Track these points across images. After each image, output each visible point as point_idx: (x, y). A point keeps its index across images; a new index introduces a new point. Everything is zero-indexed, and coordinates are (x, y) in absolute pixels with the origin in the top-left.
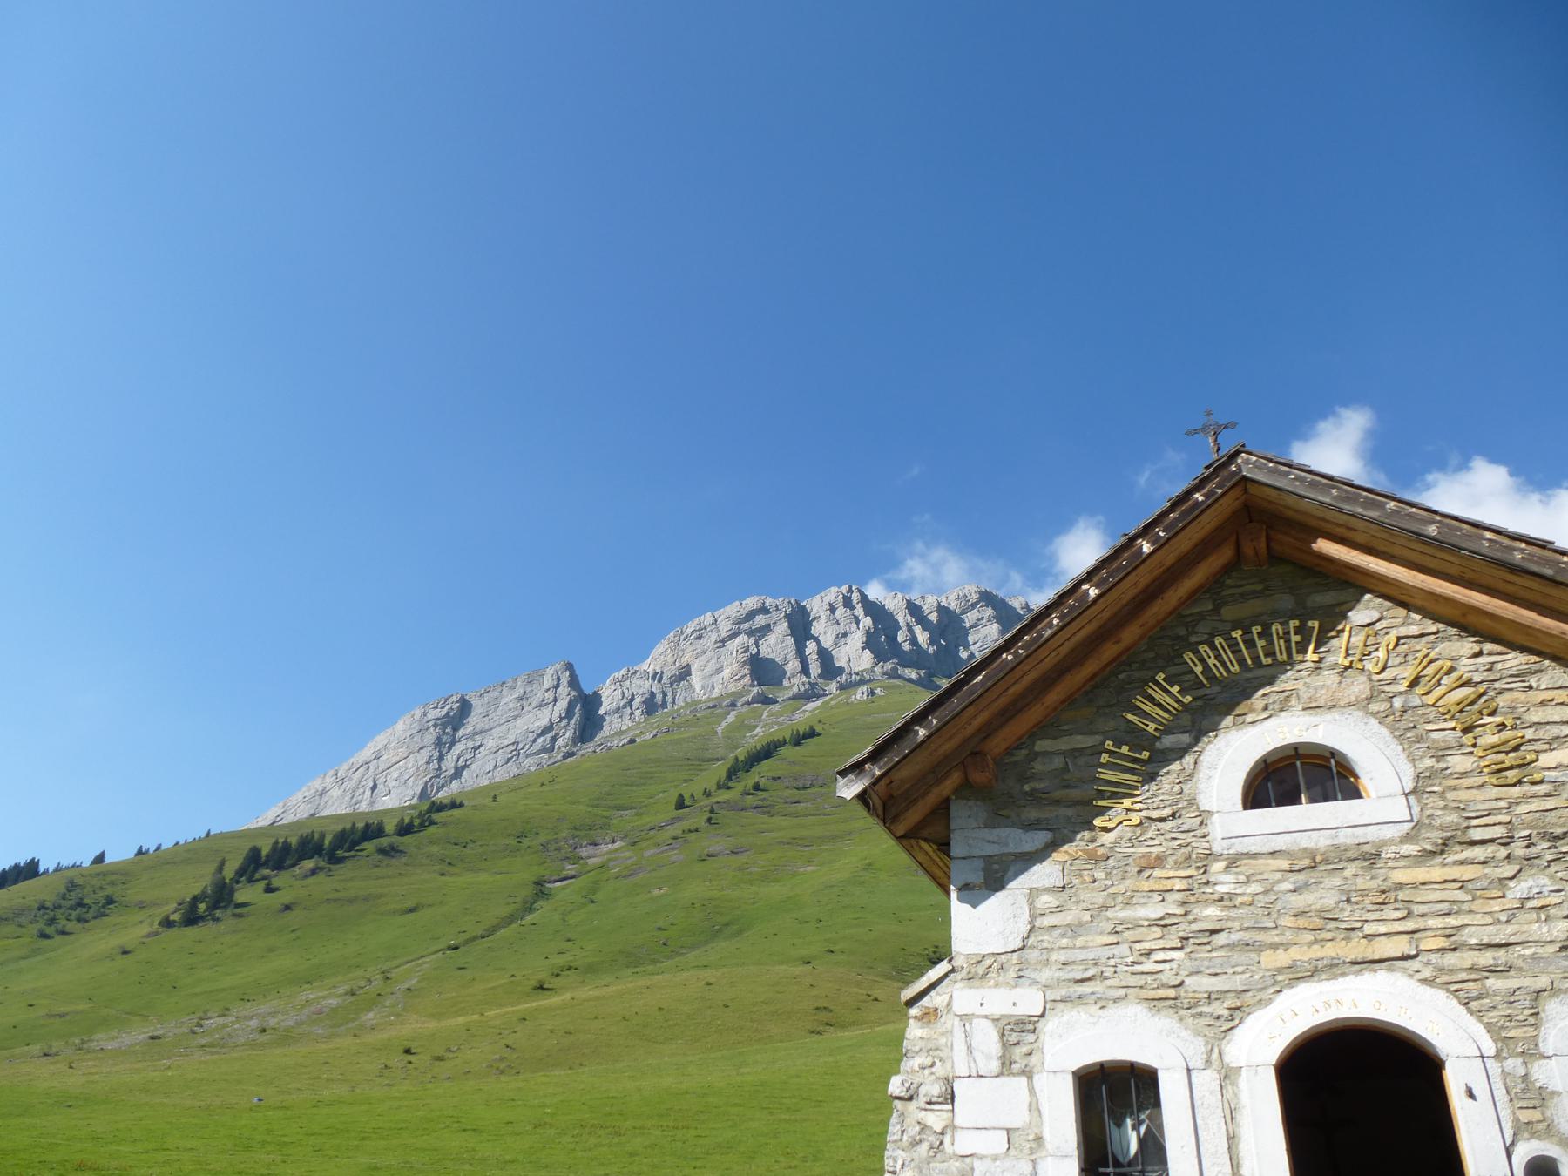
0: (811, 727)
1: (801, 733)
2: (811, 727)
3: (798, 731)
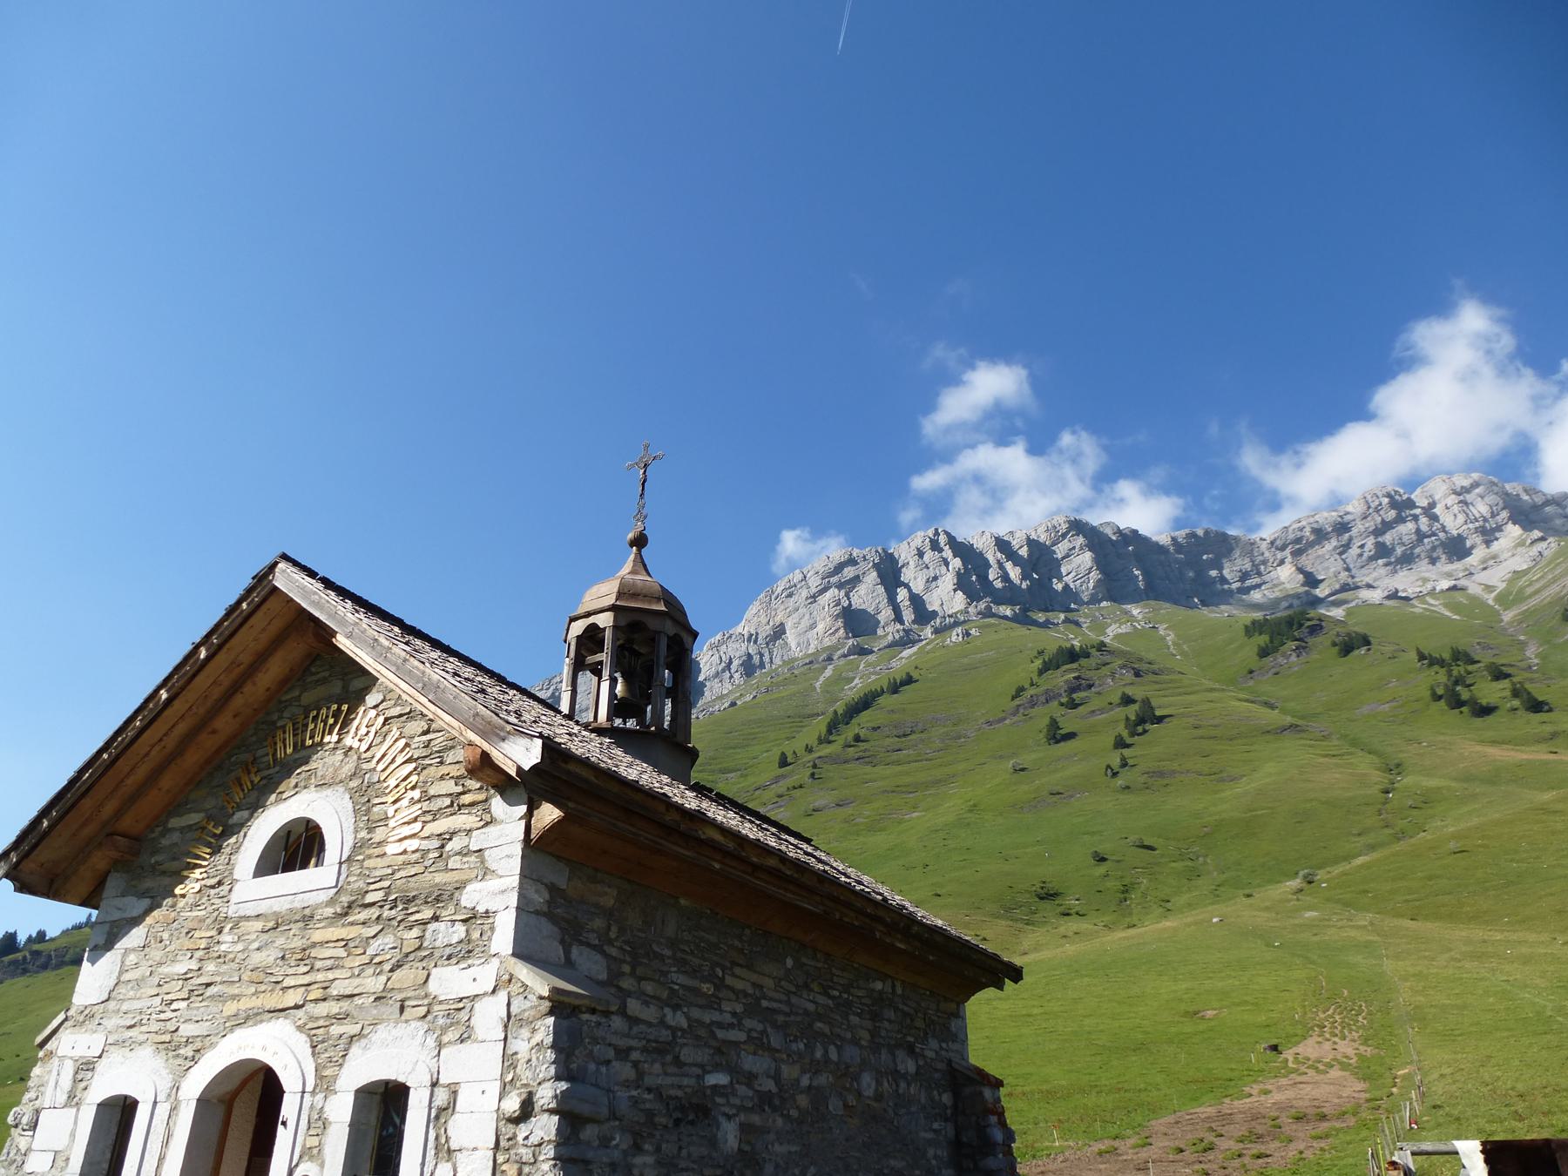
0: (908, 674)
1: (898, 681)
2: (908, 674)
3: (894, 679)
